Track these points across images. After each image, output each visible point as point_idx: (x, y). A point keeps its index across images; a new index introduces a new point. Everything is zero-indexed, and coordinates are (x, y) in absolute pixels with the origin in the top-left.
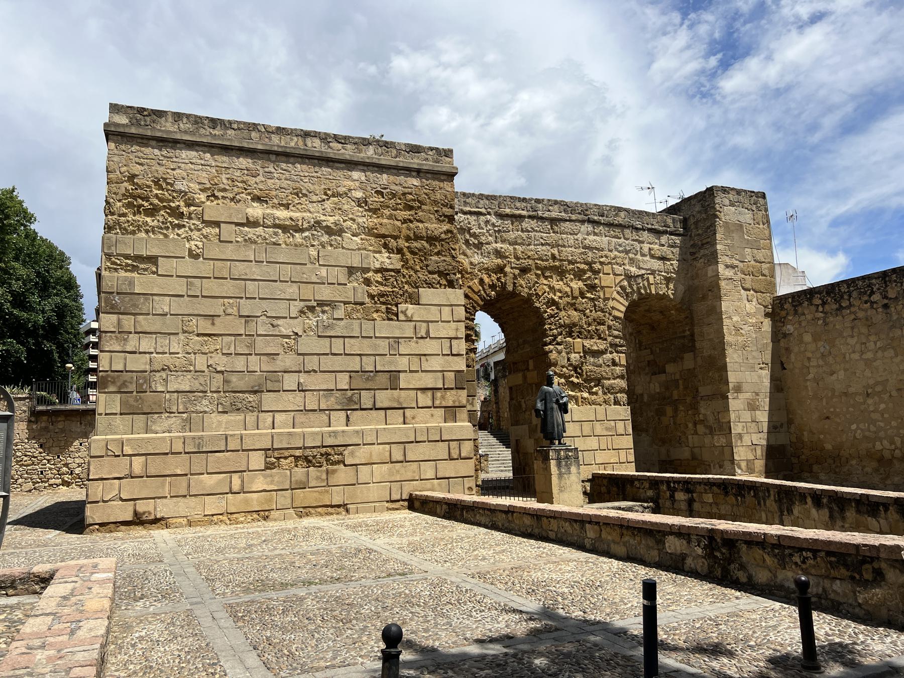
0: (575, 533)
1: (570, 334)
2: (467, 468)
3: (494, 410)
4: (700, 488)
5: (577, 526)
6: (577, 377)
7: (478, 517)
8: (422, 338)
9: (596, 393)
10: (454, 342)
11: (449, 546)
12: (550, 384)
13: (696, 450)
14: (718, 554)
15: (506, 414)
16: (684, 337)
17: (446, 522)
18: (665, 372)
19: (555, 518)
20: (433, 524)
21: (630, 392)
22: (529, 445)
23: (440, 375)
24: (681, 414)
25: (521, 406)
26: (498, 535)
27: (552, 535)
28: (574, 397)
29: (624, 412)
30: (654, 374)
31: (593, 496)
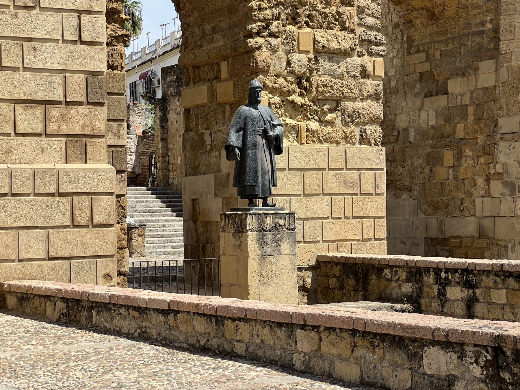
0: (278, 344)
1: (293, 20)
2: (107, 240)
3: (160, 151)
4: (487, 281)
5: (281, 333)
6: (301, 95)
7: (117, 321)
8: (26, 7)
9: (331, 123)
10: (86, 19)
11: (62, 367)
12: (254, 102)
13: (487, 223)
14: (506, 375)
15: (178, 159)
16: (483, 32)
17: (61, 330)
18: (446, 93)
19: (246, 320)
20: (37, 333)
21: (387, 124)
22: (214, 208)
23: (59, 77)
24: (467, 163)
25: (202, 141)
26: (148, 349)
27: (240, 348)
28: (293, 127)
29: (376, 156)
30: (429, 95)
31: (314, 294)
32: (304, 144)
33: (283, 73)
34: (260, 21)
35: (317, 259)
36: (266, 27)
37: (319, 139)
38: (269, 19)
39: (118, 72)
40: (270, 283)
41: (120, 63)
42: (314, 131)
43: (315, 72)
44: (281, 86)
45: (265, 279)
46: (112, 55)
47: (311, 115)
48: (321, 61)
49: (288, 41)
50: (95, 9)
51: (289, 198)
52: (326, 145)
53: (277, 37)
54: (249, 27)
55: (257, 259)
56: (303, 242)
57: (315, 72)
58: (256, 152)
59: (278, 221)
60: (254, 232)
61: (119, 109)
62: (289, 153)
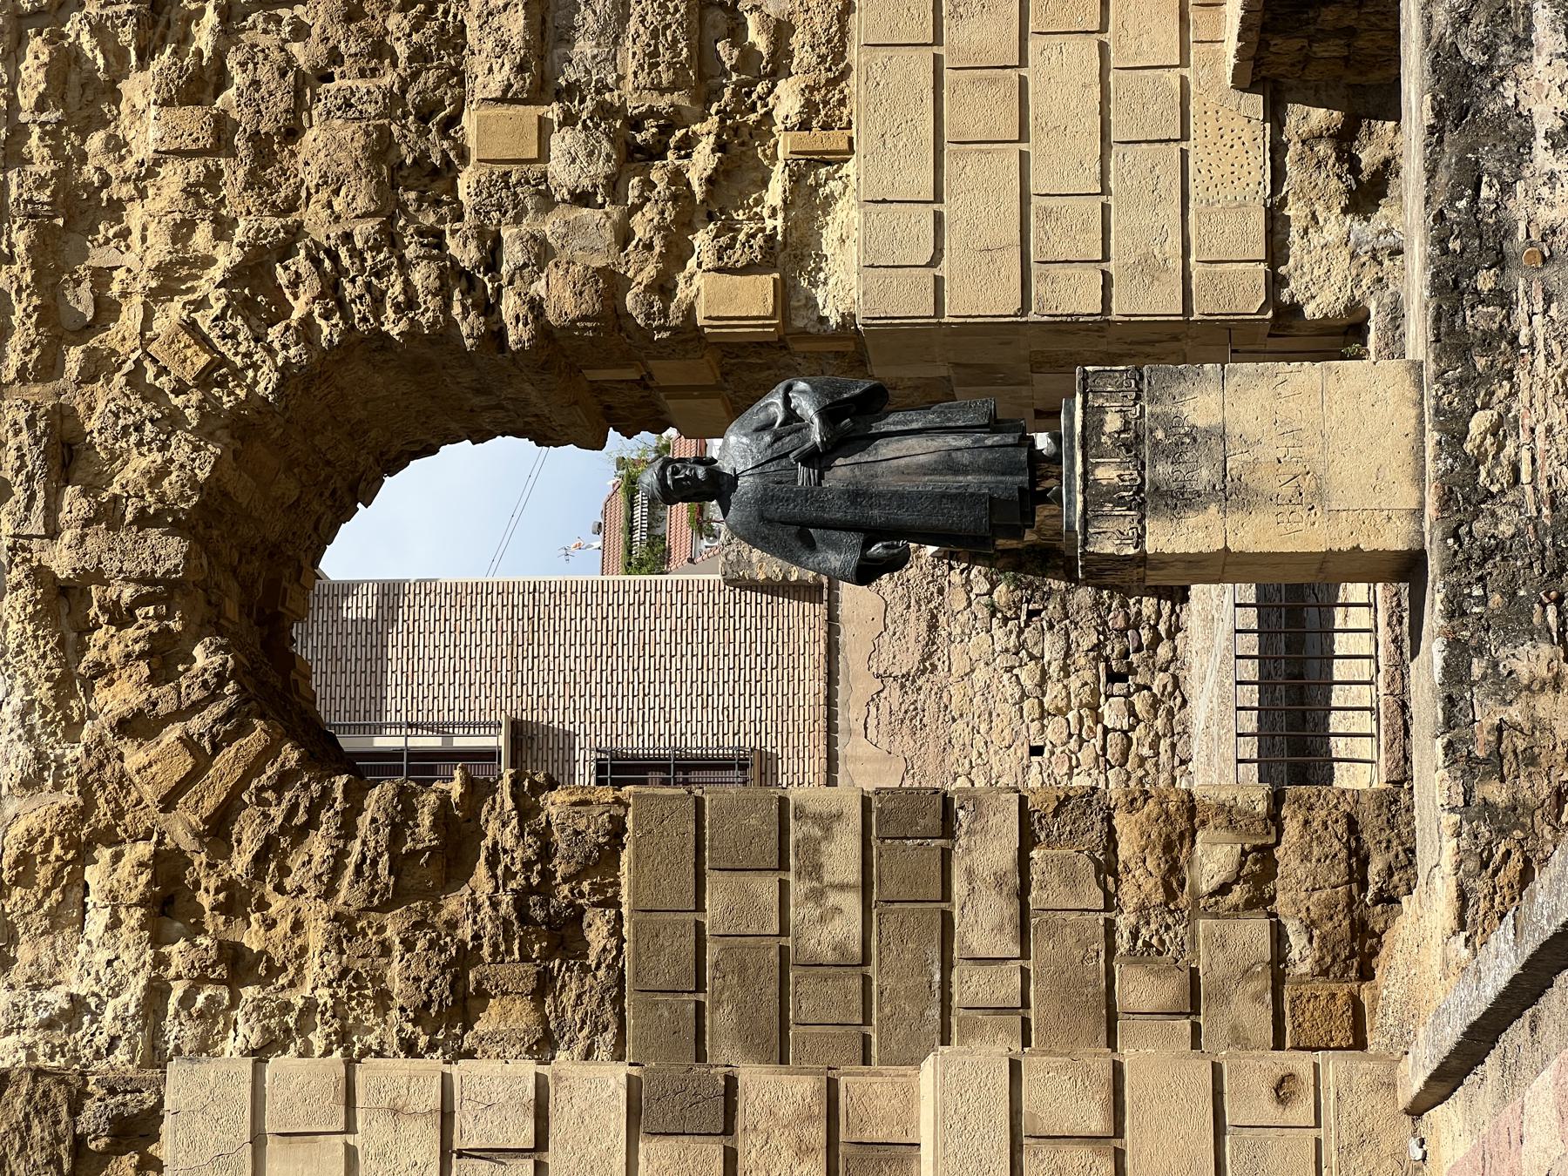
6: (687, 146)
28: (796, 178)
32: (850, 140)
33: (615, 216)
34: (447, 306)
35: (1244, 90)
36: (468, 280)
37: (833, 83)
38: (442, 270)
39: (630, 816)
40: (1320, 470)
41: (601, 809)
42: (808, 101)
43: (607, 96)
44: (658, 229)
45: (1304, 486)
46: (576, 833)
47: (753, 109)
48: (571, 74)
49: (508, 204)
50: (435, 1101)
51: (1034, 199)
52: (853, 54)
53: (498, 240)
54: (468, 342)
55: (1236, 517)
56: (1184, 145)
57: (607, 96)
58: (880, 495)
59: (1110, 435)
60: (1144, 528)
61: (749, 814)
62: (884, 201)
